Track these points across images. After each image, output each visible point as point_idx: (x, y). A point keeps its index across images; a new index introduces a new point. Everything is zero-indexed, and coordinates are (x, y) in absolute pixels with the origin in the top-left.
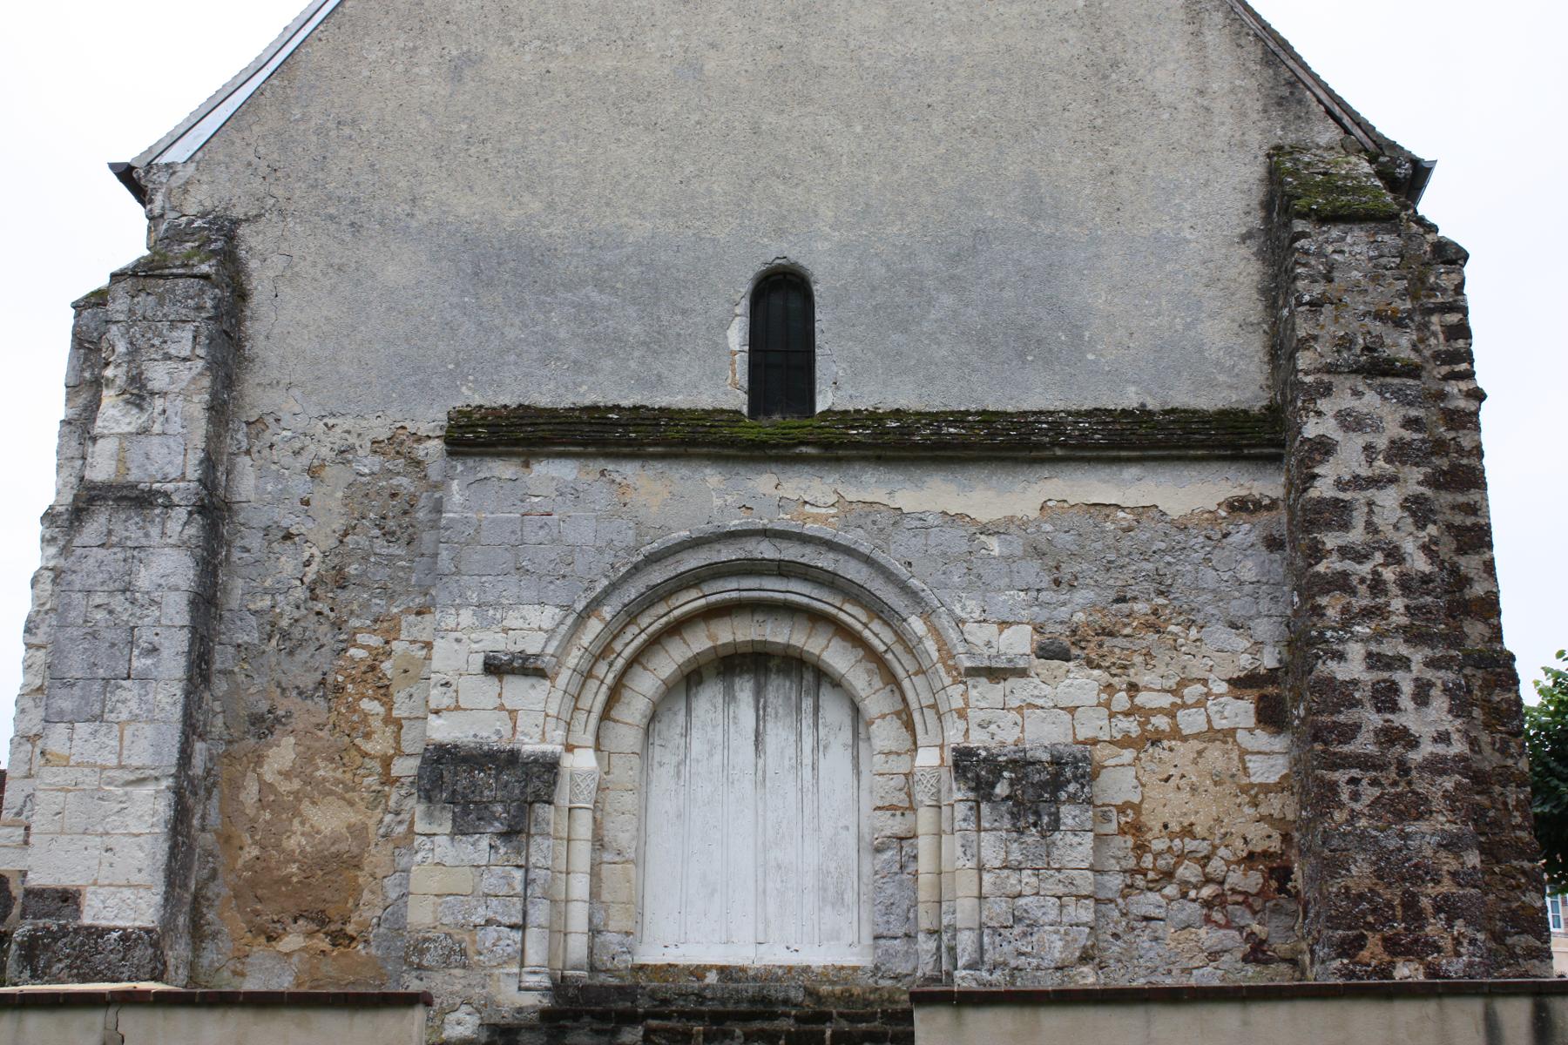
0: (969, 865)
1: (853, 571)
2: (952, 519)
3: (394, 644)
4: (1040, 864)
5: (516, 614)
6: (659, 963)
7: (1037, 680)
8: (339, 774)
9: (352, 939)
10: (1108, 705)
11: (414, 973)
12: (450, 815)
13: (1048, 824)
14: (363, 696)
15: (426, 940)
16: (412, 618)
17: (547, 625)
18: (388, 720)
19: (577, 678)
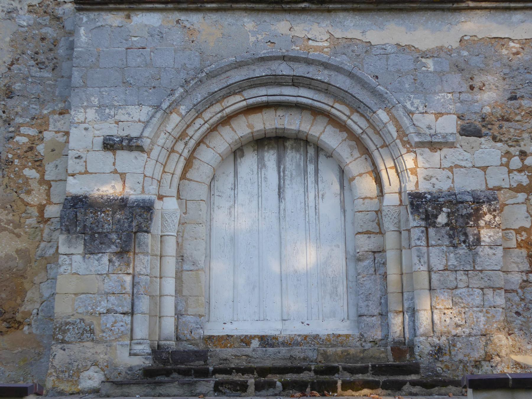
0: (422, 268)
1: (341, 81)
2: (401, 48)
3: (46, 134)
4: (468, 268)
5: (123, 111)
6: (221, 334)
7: (461, 150)
8: (10, 217)
9: (20, 323)
10: (507, 165)
11: (60, 346)
12: (82, 242)
13: (473, 242)
14: (25, 167)
15: (67, 324)
16: (56, 116)
17: (144, 118)
18: (42, 181)
19: (164, 152)
